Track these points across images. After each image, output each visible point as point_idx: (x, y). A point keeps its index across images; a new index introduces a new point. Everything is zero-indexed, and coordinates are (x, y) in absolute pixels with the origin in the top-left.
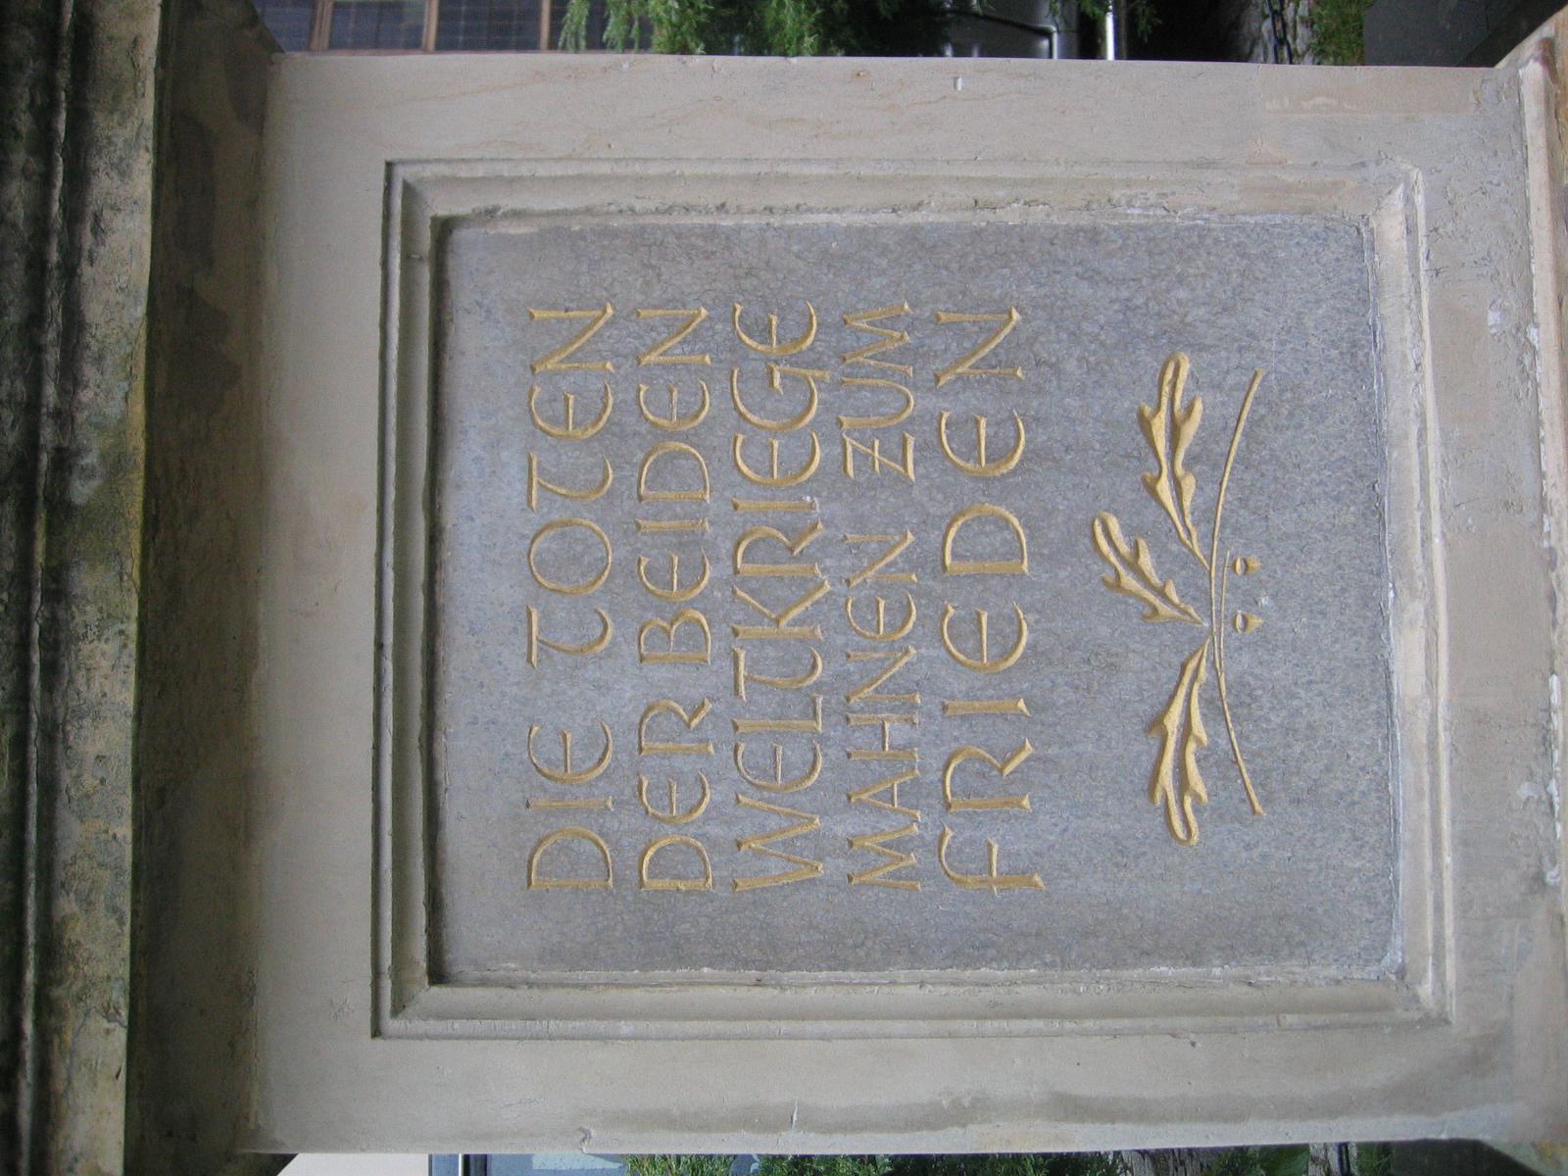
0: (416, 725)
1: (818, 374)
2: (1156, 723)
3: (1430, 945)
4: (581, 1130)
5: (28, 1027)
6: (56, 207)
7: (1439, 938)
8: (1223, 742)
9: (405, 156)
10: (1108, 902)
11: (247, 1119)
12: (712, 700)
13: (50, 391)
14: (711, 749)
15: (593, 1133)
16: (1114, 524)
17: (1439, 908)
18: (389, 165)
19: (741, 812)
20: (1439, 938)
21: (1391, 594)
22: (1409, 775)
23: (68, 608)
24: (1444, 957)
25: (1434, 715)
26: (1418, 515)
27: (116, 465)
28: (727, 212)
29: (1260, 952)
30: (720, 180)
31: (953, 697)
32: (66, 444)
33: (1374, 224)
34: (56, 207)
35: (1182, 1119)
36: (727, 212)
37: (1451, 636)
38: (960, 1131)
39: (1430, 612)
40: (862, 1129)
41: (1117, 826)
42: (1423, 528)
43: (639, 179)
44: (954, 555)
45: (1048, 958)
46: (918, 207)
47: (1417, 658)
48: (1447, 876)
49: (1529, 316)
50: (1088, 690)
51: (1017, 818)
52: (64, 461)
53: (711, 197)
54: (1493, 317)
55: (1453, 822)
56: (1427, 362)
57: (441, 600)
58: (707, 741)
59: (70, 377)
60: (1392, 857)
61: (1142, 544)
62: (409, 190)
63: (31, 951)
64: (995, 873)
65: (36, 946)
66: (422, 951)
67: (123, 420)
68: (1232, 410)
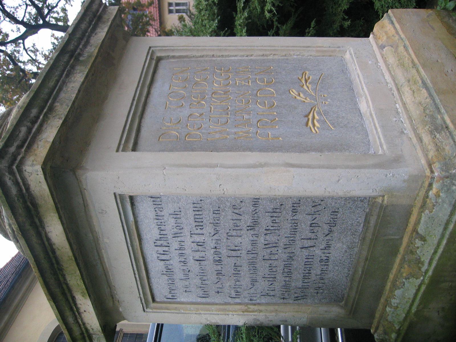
0: (139, 113)
1: (231, 74)
2: (307, 116)
3: (379, 144)
4: (164, 167)
5: (41, 117)
6: (89, 30)
7: (380, 143)
8: (322, 119)
9: (153, 45)
10: (298, 142)
11: (81, 164)
12: (205, 113)
13: (81, 46)
14: (204, 120)
15: (167, 168)
16: (294, 91)
17: (379, 138)
18: (150, 48)
19: (210, 128)
20: (380, 143)
21: (358, 99)
22: (368, 124)
23: (74, 70)
24: (383, 146)
25: (370, 111)
26: (360, 86)
27: (90, 56)
28: (214, 57)
29: (337, 150)
30: (214, 50)
31: (259, 112)
32: (81, 53)
33: (344, 57)
34: (89, 30)
35: (319, 168)
36: (214, 57)
37: (371, 99)
38: (261, 169)
39: (366, 97)
40: (236, 168)
41: (299, 130)
42: (361, 87)
43: (198, 50)
44: (259, 94)
45: (284, 151)
46: (252, 56)
47: (365, 106)
48: (380, 133)
49: (377, 62)
50: (290, 111)
51: (275, 129)
52: (80, 55)
53: (211, 53)
54: (370, 62)
55: (379, 124)
56: (358, 68)
57: (148, 101)
58: (203, 118)
59: (85, 46)
60: (368, 136)
61: (300, 93)
62: (153, 51)
63: (47, 107)
64: (270, 137)
65: (48, 107)
66: (132, 141)
67: (93, 52)
68: (318, 77)
